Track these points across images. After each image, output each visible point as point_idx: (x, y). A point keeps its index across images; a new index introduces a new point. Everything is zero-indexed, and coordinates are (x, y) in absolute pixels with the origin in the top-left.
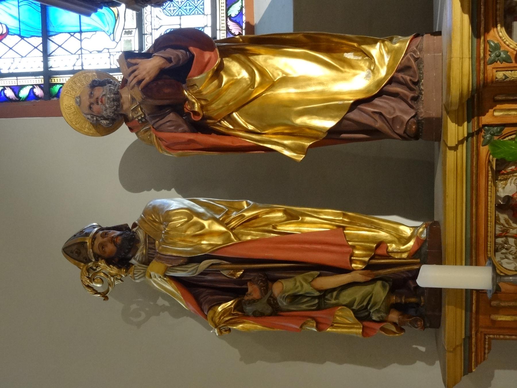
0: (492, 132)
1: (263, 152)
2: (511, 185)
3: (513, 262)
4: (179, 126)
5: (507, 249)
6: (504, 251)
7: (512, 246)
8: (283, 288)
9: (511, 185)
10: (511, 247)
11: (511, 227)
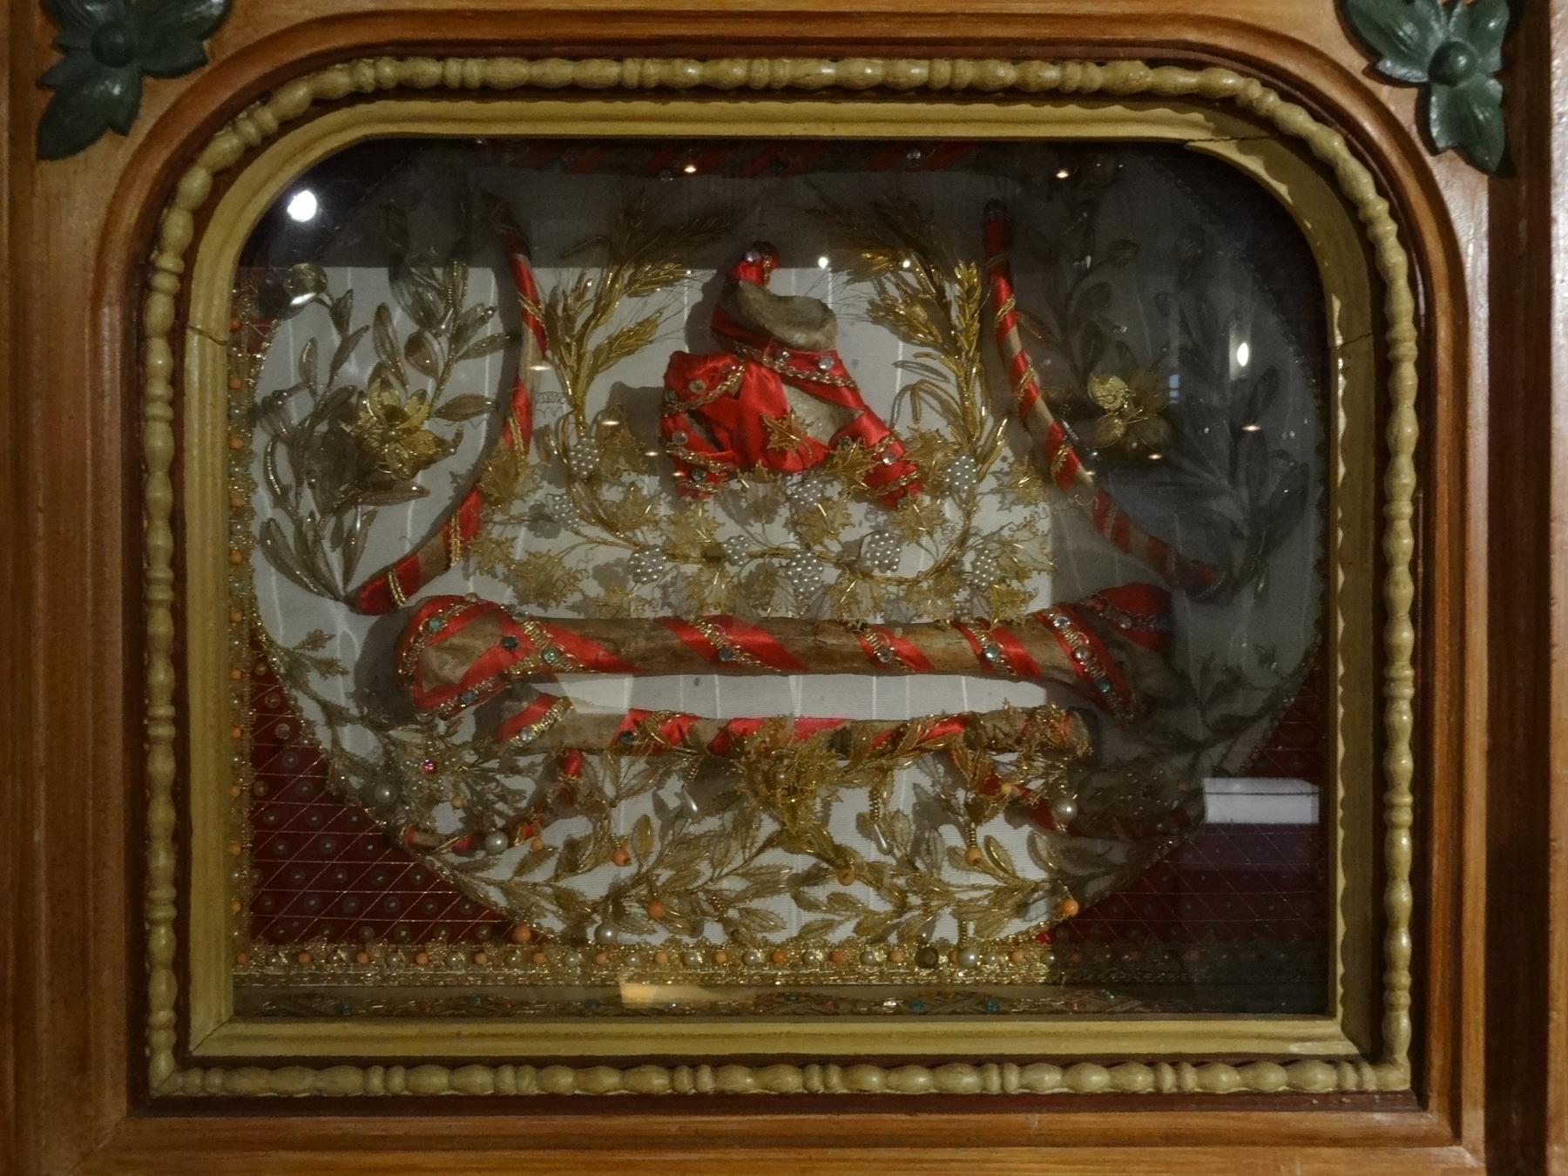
0: (1462, 61)
1: (1434, 99)
2: (896, 365)
3: (321, 388)
4: (807, 807)
5: (415, 345)
6: (402, 324)
7: (441, 382)
8: (1065, 684)
9: (896, 365)
10: (428, 371)
11: (584, 372)
